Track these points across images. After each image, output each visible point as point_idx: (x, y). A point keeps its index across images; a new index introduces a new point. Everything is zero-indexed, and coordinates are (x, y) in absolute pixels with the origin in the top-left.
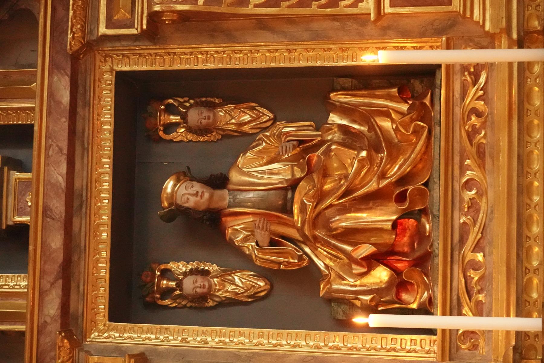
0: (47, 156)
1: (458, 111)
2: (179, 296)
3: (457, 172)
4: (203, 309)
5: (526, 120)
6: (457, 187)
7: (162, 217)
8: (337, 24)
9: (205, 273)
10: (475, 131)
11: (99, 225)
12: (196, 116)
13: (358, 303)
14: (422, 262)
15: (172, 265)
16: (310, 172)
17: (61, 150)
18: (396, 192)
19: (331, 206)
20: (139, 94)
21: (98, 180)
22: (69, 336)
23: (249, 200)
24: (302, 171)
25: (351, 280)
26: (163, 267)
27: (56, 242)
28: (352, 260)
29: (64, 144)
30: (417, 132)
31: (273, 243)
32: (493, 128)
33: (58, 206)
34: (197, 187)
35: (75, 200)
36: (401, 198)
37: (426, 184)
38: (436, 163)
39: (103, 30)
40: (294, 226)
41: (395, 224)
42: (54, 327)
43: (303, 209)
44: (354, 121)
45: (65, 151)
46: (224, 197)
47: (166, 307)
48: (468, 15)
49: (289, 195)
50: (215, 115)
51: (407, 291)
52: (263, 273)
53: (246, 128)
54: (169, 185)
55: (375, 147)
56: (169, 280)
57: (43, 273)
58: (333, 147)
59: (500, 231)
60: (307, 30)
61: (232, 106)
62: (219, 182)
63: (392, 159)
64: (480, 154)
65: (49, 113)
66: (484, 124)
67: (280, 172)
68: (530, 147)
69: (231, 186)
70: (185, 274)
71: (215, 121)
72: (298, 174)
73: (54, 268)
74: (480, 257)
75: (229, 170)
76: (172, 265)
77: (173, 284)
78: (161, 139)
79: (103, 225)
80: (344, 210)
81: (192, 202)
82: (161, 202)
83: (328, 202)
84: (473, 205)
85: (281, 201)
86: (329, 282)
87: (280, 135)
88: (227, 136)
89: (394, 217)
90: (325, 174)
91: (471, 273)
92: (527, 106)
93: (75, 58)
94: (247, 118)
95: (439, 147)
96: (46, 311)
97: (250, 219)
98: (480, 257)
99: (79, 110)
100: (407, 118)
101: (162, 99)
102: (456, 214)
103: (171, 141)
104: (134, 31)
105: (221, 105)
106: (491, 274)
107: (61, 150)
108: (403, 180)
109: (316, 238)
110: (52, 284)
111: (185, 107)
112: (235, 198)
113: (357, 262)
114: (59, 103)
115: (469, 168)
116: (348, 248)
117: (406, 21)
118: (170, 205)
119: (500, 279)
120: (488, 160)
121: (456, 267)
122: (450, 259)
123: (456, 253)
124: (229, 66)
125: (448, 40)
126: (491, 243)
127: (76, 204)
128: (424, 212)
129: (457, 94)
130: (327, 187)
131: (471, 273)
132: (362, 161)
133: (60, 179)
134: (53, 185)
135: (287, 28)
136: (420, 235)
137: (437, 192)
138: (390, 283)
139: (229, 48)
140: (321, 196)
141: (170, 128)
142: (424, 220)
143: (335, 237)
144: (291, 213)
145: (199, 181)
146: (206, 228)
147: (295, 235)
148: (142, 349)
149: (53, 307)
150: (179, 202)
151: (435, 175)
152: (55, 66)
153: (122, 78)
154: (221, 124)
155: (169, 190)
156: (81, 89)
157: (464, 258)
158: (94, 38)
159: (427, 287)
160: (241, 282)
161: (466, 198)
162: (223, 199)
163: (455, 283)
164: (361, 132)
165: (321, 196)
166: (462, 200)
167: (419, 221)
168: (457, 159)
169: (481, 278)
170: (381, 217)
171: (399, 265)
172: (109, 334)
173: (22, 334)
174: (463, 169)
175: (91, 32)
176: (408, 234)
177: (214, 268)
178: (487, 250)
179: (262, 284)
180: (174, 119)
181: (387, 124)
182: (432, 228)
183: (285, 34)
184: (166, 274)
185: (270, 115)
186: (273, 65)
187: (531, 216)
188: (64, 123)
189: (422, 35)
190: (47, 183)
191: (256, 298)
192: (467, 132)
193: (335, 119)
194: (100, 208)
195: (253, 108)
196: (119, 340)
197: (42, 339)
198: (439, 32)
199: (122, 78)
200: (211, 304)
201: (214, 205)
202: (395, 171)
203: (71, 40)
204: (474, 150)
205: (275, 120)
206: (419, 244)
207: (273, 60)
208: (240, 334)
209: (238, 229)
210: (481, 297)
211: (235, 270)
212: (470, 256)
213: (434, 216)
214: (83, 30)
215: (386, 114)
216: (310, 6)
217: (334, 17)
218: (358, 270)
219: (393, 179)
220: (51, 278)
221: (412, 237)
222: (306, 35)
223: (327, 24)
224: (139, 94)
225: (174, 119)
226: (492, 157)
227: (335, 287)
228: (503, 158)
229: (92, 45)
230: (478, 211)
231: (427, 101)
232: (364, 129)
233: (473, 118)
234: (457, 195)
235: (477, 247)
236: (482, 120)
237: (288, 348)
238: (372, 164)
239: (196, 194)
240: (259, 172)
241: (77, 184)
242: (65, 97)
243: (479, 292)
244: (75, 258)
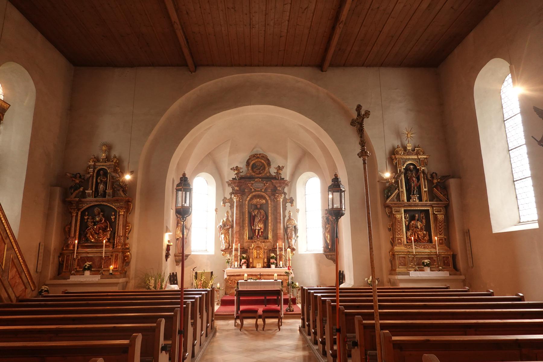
85: (417, 227)
240: (419, 224)
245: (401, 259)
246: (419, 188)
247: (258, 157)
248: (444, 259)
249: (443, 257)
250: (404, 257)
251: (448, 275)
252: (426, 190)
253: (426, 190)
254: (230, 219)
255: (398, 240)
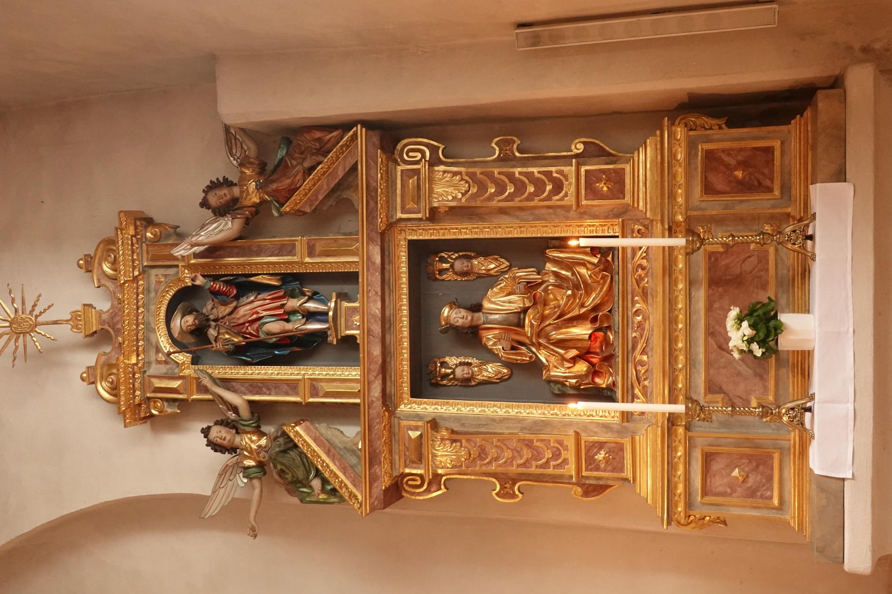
0: (368, 297)
1: (630, 266)
2: (452, 379)
3: (630, 305)
4: (469, 388)
5: (674, 276)
6: (630, 314)
7: (441, 332)
8: (551, 210)
9: (469, 364)
10: (641, 279)
11: (402, 338)
12: (458, 265)
13: (567, 383)
14: (609, 359)
15: (447, 359)
16: (535, 304)
17: (376, 293)
18: (592, 316)
19: (550, 324)
20: (422, 252)
21: (400, 309)
22: (387, 410)
23: (496, 319)
24: (530, 301)
25: (563, 370)
26: (441, 360)
27: (377, 351)
28: (563, 359)
29: (379, 290)
30: (603, 278)
31: (513, 348)
32: (652, 278)
33: (377, 329)
34: (463, 312)
35: (387, 323)
36: (594, 320)
37: (610, 311)
38: (616, 298)
39: (400, 215)
40: (525, 335)
41: (590, 336)
42: (378, 404)
43: (532, 325)
44: (562, 269)
45: (380, 294)
46: (480, 317)
47: (445, 385)
48: (636, 206)
49: (522, 316)
50: (472, 264)
51: (599, 377)
52: (506, 364)
53: (492, 272)
54: (446, 311)
55: (576, 287)
56: (446, 368)
57: (369, 370)
58: (550, 287)
59: (657, 341)
60: (531, 214)
61: (482, 259)
62: (477, 308)
63: (588, 294)
64: (645, 295)
65: (368, 270)
66: (646, 274)
67: (515, 302)
68: (676, 293)
69: (484, 311)
70: (457, 366)
71: (472, 268)
72: (528, 304)
73: (376, 367)
74: (645, 358)
75: (482, 300)
76: (447, 359)
77: (449, 371)
78: (437, 279)
79: (404, 337)
80: (558, 328)
81: (460, 322)
82: (440, 322)
83: (548, 323)
84: (640, 325)
85: (517, 320)
86: (548, 370)
87: (514, 278)
88: (480, 276)
89: (590, 332)
90: (545, 304)
91: (639, 368)
92: (674, 267)
93: (383, 234)
94: (492, 266)
95: (617, 289)
96: (372, 394)
97: (497, 332)
98: (645, 358)
99: (387, 266)
100: (597, 269)
101: (436, 253)
102: (630, 331)
103: (443, 280)
104: (419, 216)
105: (475, 258)
106: (652, 369)
107: (376, 293)
108: (596, 308)
109: (540, 344)
110: (242, 208)
111: (452, 259)
112: (487, 318)
113: (568, 361)
114: (374, 263)
115: (637, 302)
116: (562, 352)
117: (596, 209)
118: (446, 324)
119: (657, 375)
120: (649, 297)
121: (630, 364)
122: (626, 360)
123: (630, 355)
124: (481, 236)
125: (623, 221)
126: (652, 350)
127: (387, 326)
128: (609, 328)
129: (629, 256)
130: (547, 312)
131: (639, 368)
132: (568, 296)
133: (377, 311)
134: (373, 316)
135: (518, 213)
136: (606, 340)
137: (617, 318)
138: (588, 371)
139: (481, 225)
140: (543, 318)
141: (442, 271)
142: (609, 333)
143: (552, 344)
144: (523, 327)
145: (464, 308)
146: (469, 337)
147: (527, 341)
148: (433, 415)
149: (376, 392)
150: (452, 322)
151: (616, 306)
152: (370, 239)
153: (412, 244)
154: (476, 270)
155: (446, 314)
156: (387, 253)
157: (635, 358)
158: (394, 220)
159: (611, 375)
160: (491, 370)
161: (636, 322)
162: (479, 319)
163: (630, 374)
164: (567, 276)
165: (543, 318)
166: (633, 323)
167: (606, 334)
168: (630, 297)
169: (647, 371)
170: (582, 331)
171: (594, 360)
172: (410, 407)
173: (357, 405)
174: (634, 303)
175: (392, 217)
176: (599, 340)
177: (474, 361)
178: (650, 354)
179: (505, 371)
180: (445, 266)
181: (583, 271)
182: (614, 339)
183: (517, 217)
184: (444, 364)
185: (508, 264)
186: (510, 236)
187: (677, 336)
188: (378, 276)
189: (607, 217)
190: (369, 314)
191: (502, 380)
192: (636, 280)
193: (550, 267)
194: (402, 327)
195: (496, 259)
196: (419, 410)
197: (371, 411)
198: (617, 216)
199: (412, 244)
200: (473, 383)
201: (474, 323)
202: (590, 302)
203: (381, 222)
204: (640, 291)
205: (510, 267)
206: (606, 347)
207: (510, 232)
208: (494, 406)
209: (490, 338)
210: (646, 383)
211: (488, 362)
212: (638, 357)
213: (615, 332)
214: (387, 217)
215: (583, 264)
216: (533, 200)
217: (549, 207)
218: (567, 365)
219: (589, 308)
220: (375, 374)
221: (601, 343)
222: (531, 218)
223: (544, 211)
224: (422, 252)
225: (445, 266)
226: (652, 296)
227: (552, 373)
228: (660, 298)
229: (391, 225)
230: (643, 329)
231: (610, 258)
232: (569, 274)
233: (640, 270)
234: (630, 319)
235: (644, 352)
236: (645, 272)
237: (525, 414)
238: (575, 298)
239: (463, 318)
240: (500, 303)
241: (387, 313)
242: (378, 260)
243: (645, 380)
244: (388, 360)
245: (718, 483)
246: (293, 282)
247: (561, 445)
248: (718, 182)
249: (708, 189)
250: (708, 458)
251: (845, 189)
252: (301, 243)
253: (301, 243)
254: (791, 273)
255: (591, 463)
